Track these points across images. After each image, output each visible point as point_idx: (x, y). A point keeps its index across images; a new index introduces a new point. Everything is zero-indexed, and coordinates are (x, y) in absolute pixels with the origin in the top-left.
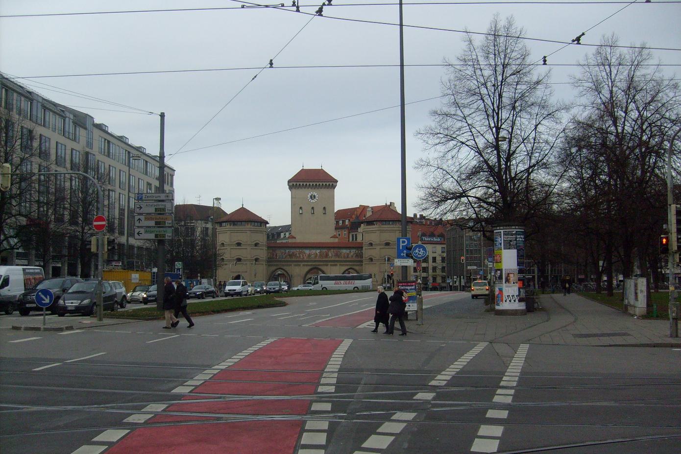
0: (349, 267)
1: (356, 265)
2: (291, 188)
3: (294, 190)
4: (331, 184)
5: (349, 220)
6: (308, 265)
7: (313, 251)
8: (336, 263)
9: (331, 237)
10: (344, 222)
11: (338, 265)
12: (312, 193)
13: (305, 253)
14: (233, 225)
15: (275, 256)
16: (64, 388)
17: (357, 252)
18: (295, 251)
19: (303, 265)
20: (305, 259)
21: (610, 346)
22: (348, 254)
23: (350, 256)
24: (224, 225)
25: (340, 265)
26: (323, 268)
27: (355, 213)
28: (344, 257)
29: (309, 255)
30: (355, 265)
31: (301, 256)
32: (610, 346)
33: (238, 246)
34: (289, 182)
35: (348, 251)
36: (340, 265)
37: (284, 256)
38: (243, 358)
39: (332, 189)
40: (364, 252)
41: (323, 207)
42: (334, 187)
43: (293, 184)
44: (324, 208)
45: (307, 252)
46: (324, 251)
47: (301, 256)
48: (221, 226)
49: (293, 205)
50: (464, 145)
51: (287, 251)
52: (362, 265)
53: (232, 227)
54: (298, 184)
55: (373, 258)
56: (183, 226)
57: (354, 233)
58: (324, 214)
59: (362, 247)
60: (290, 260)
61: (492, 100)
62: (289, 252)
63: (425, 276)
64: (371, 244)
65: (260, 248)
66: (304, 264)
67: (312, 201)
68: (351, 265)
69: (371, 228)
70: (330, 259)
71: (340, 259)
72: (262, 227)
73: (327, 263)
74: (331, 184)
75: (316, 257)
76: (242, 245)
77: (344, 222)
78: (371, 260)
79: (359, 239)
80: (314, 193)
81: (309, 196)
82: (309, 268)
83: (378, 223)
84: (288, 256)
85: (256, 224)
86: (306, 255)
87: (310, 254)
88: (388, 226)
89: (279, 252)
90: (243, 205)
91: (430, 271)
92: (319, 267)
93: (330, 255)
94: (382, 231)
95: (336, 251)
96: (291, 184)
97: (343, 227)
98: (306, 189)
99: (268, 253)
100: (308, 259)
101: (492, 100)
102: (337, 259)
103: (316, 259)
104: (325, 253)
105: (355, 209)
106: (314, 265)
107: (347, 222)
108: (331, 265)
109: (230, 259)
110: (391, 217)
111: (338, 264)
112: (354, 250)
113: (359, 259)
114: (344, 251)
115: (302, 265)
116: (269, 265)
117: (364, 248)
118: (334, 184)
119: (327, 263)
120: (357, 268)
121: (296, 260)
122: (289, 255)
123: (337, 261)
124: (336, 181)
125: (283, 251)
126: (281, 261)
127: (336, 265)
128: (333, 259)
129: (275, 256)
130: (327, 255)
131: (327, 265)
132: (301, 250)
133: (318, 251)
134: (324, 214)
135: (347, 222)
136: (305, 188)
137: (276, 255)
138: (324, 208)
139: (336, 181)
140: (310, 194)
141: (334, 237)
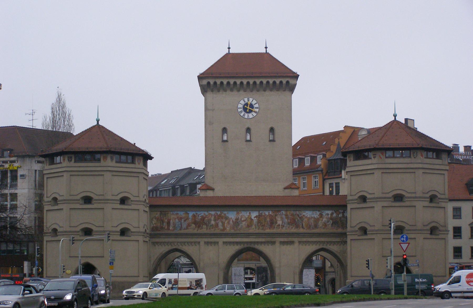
0: (321, 246)
1: (334, 243)
2: (204, 89)
3: (210, 94)
4: (284, 81)
5: (324, 156)
6: (234, 243)
7: (245, 214)
8: (290, 239)
9: (285, 188)
10: (313, 159)
12: (246, 100)
13: (227, 218)
14: (75, 162)
15: (165, 224)
16: (415, 303)
17: (335, 215)
18: (206, 213)
20: (228, 230)
22: (317, 220)
23: (320, 224)
24: (58, 161)
25: (300, 242)
27: (337, 141)
28: (309, 227)
29: (237, 222)
30: (331, 242)
31: (220, 224)
33: (85, 203)
34: (200, 78)
35: (316, 214)
36: (300, 242)
37: (184, 226)
39: (287, 93)
40: (348, 214)
41: (270, 126)
42: (291, 88)
43: (209, 83)
44: (272, 130)
45: (232, 215)
47: (220, 224)
48: (52, 163)
49: (208, 122)
51: (191, 214)
52: (345, 242)
53: (72, 164)
54: (218, 82)
55: (369, 228)
56: (189, 225)
57: (334, 181)
58: (270, 141)
59: (345, 206)
60: (195, 231)
62: (194, 216)
64: (363, 199)
65: (133, 207)
67: (246, 117)
68: (323, 242)
69: (361, 164)
70: (279, 231)
71: (301, 230)
72: (137, 165)
73: (273, 240)
74: (284, 81)
75: (249, 226)
76: (93, 202)
77: (313, 159)
78: (364, 231)
79: (344, 191)
80: (251, 100)
81: (240, 106)
82: (237, 248)
83: (379, 153)
84: (193, 226)
85: (123, 158)
87: (237, 219)
88: (401, 160)
89: (173, 216)
90: (98, 121)
92: (257, 247)
93: (280, 222)
94: (386, 171)
95: (292, 215)
96: (205, 82)
97: (313, 170)
98: (235, 93)
99: (151, 220)
100: (232, 231)
102: (294, 230)
103: (251, 231)
105: (336, 134)
107: (320, 161)
109: (69, 229)
110: (408, 141)
111: (296, 240)
112: (329, 212)
113: (340, 230)
114: (308, 214)
116: (154, 244)
117: (349, 207)
118: (292, 81)
119: (273, 240)
120: (334, 248)
121: (208, 232)
122: (195, 223)
123: (293, 235)
124: (296, 76)
125: (181, 214)
126: (177, 235)
127: (292, 243)
128: (284, 230)
129: (165, 224)
130: (272, 223)
131: (273, 243)
132: (219, 213)
133: (254, 214)
134: (270, 141)
135: (320, 161)
136: (232, 90)
137: (169, 223)
138: (272, 130)
139: (296, 76)
140: (242, 102)
141: (323, 212)
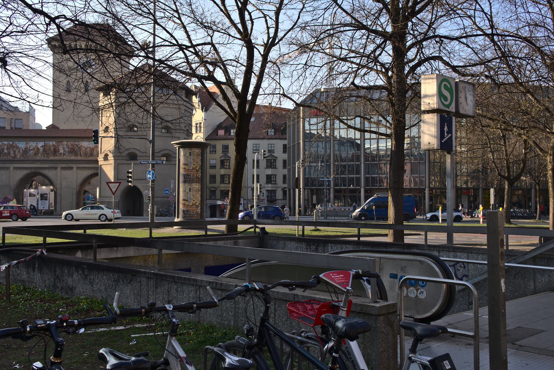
8: (70, 165)
11: (75, 169)
19: (15, 168)
21: (258, 18)
25: (78, 168)
26: (50, 174)
29: (26, 151)
31: (12, 152)
32: (258, 18)
36: (78, 168)
38: (532, 251)
45: (22, 145)
46: (51, 143)
47: (12, 152)
50: (294, 94)
61: (167, 43)
63: (270, 189)
66: (63, 166)
86: (19, 151)
87: (26, 148)
91: (280, 180)
92: (42, 171)
101: (167, 43)
102: (73, 158)
103: (38, 158)
104: (52, 149)
106: (34, 168)
108: (62, 168)
111: (74, 166)
115: (11, 169)
127: (71, 168)
130: (56, 151)
132: (11, 143)
133: (40, 144)
